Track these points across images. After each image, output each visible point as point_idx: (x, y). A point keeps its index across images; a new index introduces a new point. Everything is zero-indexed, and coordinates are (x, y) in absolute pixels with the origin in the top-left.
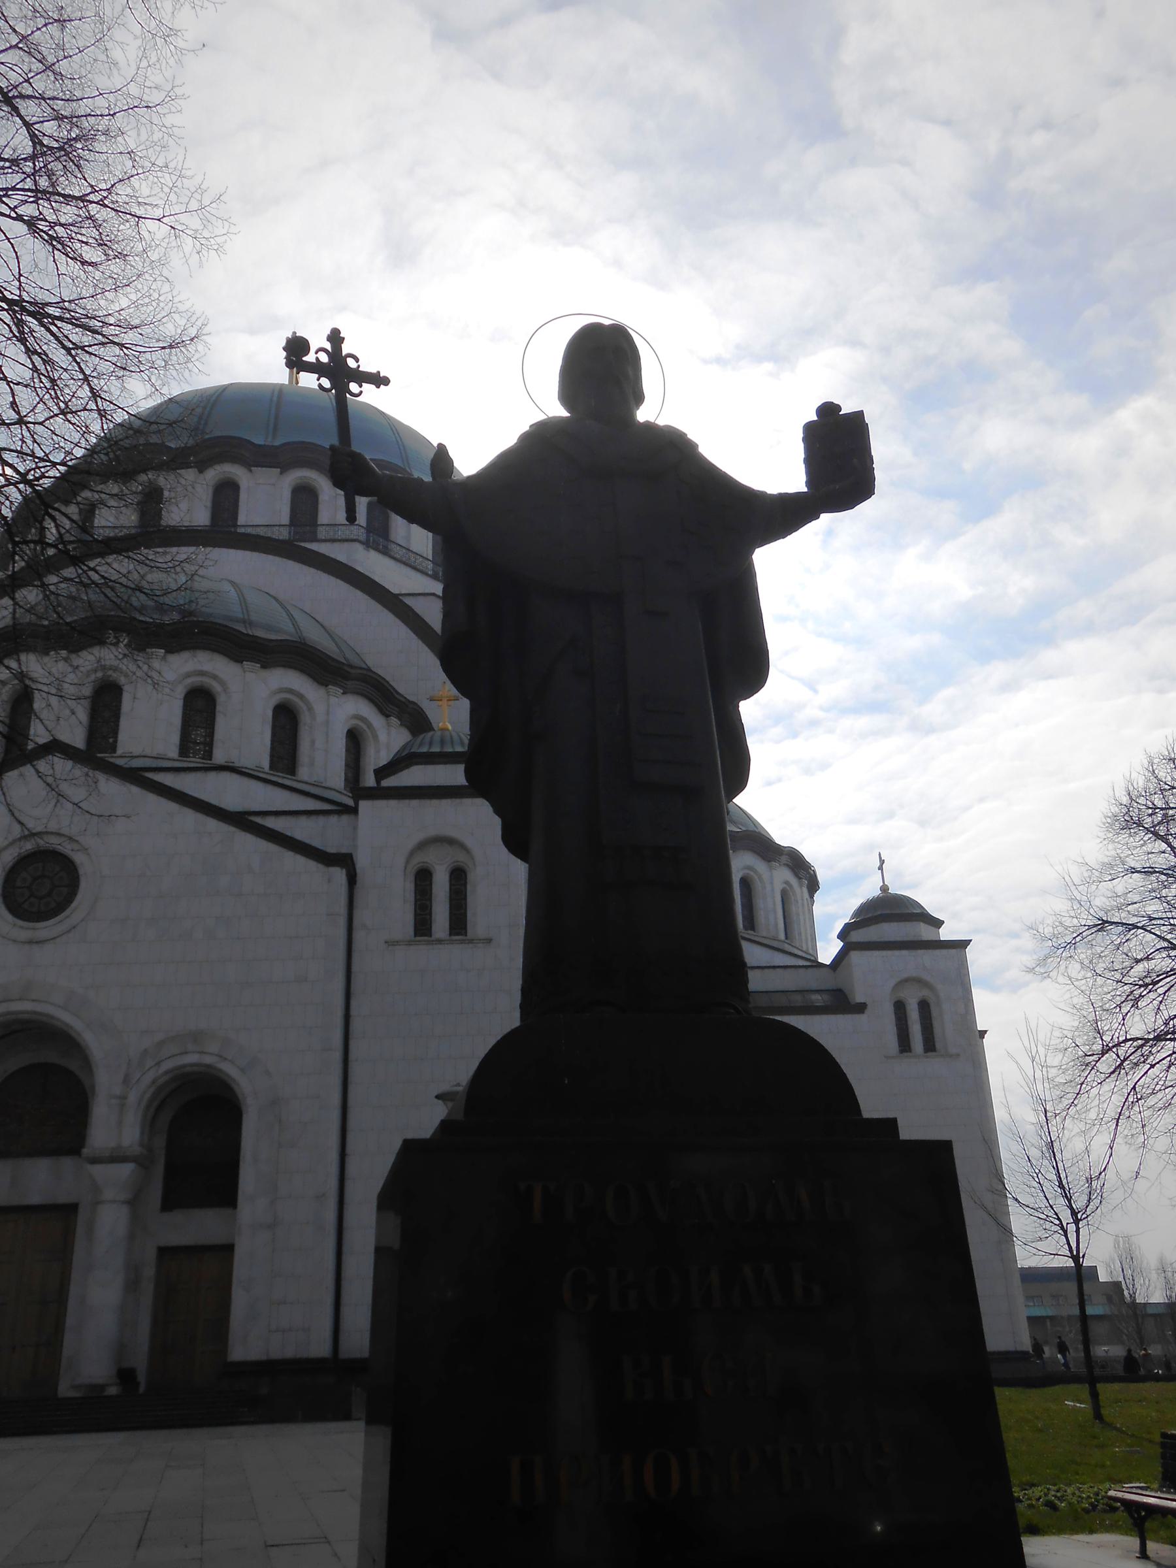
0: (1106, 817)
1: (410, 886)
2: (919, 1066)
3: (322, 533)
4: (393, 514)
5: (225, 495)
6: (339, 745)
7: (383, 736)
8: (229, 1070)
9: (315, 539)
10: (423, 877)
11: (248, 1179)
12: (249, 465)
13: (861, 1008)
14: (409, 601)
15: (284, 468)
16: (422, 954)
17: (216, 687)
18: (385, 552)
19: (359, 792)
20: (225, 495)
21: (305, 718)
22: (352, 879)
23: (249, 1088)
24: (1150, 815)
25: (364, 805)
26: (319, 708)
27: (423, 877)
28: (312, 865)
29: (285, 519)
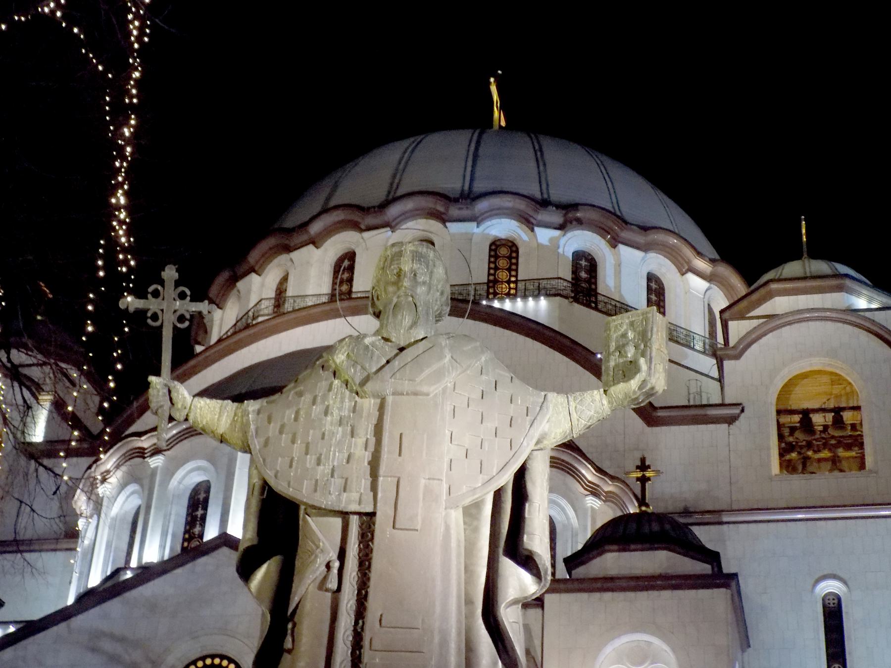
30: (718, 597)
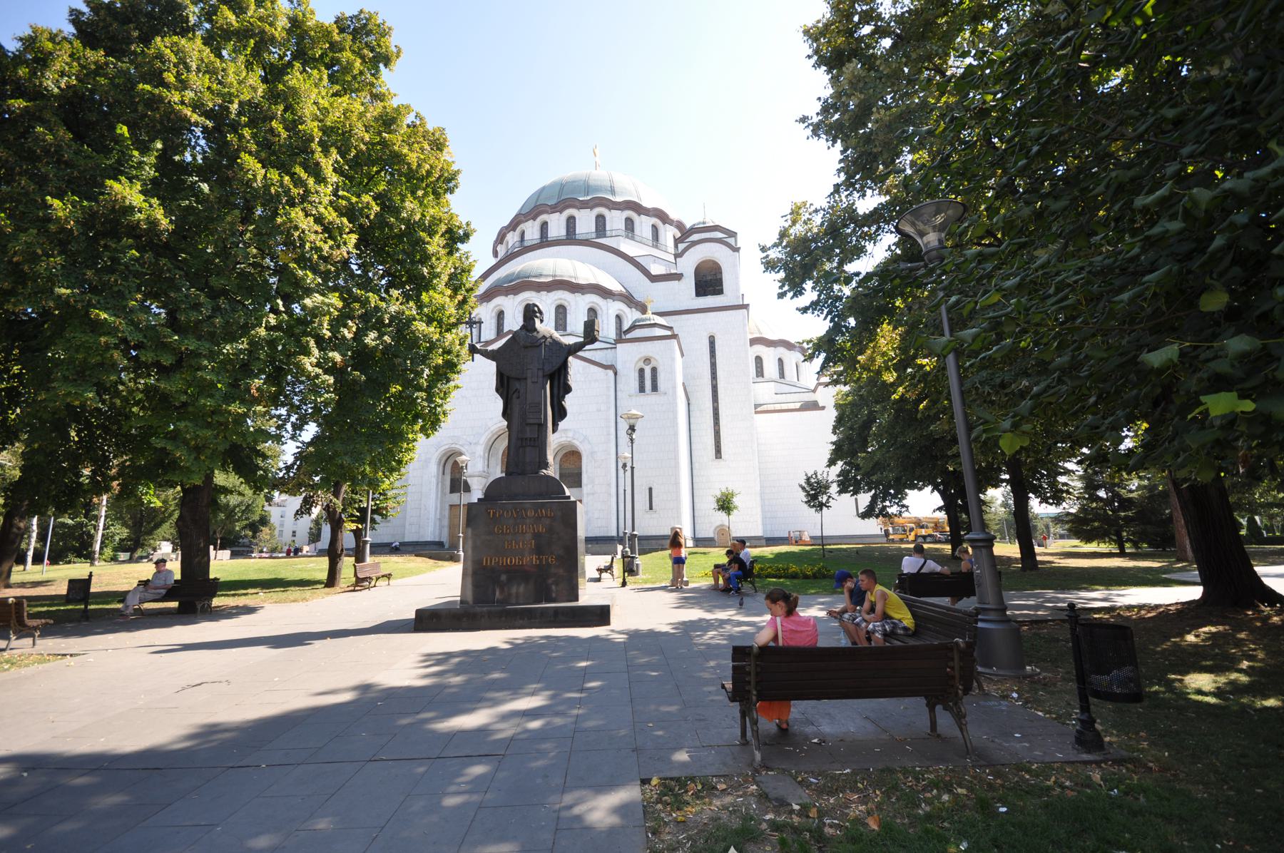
0: (468, 224)
1: (637, 375)
2: (649, 399)
3: (608, 233)
4: (1247, 348)
5: (571, 222)
6: (613, 321)
7: (629, 316)
8: (576, 443)
9: (605, 236)
10: (641, 371)
11: (585, 479)
12: (579, 208)
13: (823, 408)
14: (637, 259)
15: (591, 208)
16: (643, 399)
17: (566, 304)
18: (632, 238)
19: (620, 340)
20: (571, 222)
21: (599, 312)
22: (616, 374)
23: (583, 449)
24: (920, 308)
25: (618, 345)
26: (604, 308)
27: (641, 371)
28: (600, 369)
29: (594, 230)
30: (674, 342)
